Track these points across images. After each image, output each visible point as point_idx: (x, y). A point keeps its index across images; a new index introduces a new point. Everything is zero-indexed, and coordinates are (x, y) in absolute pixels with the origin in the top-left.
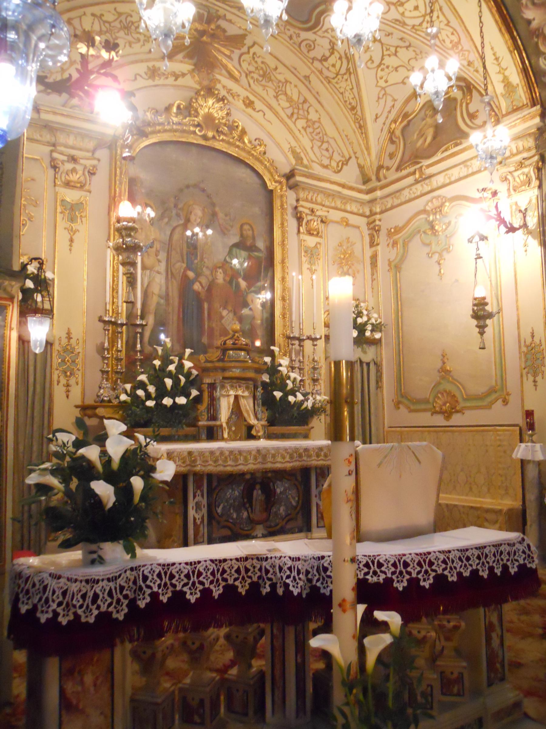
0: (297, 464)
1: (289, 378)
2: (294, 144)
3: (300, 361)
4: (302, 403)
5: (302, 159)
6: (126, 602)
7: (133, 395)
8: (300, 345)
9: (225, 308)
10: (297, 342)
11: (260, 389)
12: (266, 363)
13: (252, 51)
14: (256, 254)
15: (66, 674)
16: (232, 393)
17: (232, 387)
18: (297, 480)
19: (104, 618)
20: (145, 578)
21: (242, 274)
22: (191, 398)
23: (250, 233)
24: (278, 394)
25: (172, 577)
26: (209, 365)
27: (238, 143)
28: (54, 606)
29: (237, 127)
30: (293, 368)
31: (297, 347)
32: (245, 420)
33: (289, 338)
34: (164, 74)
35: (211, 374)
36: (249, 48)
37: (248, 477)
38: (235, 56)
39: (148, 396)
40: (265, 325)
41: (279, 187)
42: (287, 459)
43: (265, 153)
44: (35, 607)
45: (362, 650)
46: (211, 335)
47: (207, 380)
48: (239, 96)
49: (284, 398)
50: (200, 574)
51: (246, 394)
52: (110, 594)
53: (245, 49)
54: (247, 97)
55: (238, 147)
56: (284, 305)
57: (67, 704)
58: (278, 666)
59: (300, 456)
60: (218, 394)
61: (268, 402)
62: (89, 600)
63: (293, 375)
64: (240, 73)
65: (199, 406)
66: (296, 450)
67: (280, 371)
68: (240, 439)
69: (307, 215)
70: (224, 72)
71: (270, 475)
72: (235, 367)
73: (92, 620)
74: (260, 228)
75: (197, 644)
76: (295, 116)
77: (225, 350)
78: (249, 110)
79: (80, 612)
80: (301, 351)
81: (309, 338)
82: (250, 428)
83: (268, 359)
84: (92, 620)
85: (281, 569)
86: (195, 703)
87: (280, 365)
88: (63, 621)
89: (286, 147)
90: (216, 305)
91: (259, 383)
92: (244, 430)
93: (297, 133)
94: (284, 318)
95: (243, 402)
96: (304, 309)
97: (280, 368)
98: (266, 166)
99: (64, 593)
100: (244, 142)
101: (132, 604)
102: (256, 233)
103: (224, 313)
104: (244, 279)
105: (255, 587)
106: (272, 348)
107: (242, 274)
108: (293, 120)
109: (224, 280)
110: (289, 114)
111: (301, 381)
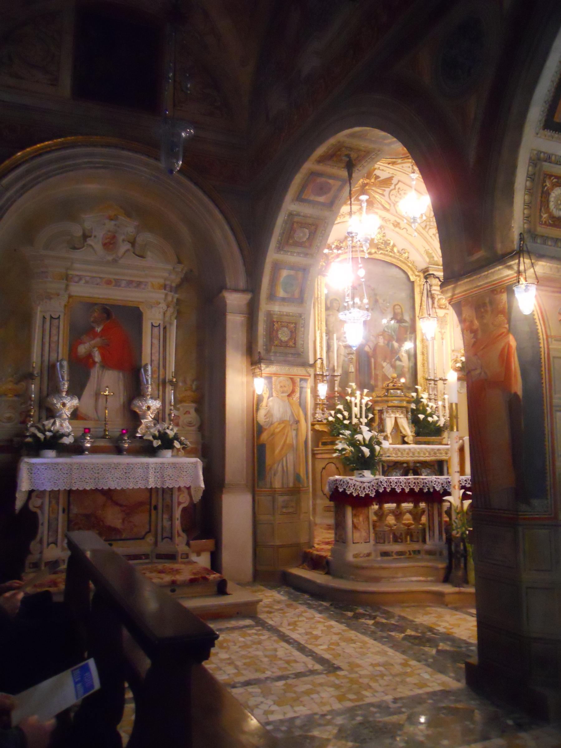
0: (433, 458)
1: (428, 406)
2: (427, 247)
3: (435, 395)
4: (437, 421)
5: (433, 257)
6: (375, 491)
7: (336, 417)
8: (435, 384)
9: (385, 361)
10: (432, 382)
11: (410, 413)
12: (413, 397)
13: (397, 187)
14: (404, 324)
15: (354, 516)
16: (393, 415)
17: (393, 412)
18: (435, 469)
19: (367, 495)
20: (381, 482)
21: (395, 338)
22: (369, 418)
23: (399, 311)
24: (421, 416)
25: (390, 483)
26: (379, 399)
27: (391, 254)
28: (352, 489)
29: (390, 243)
30: (430, 399)
31: (433, 385)
32: (401, 433)
33: (427, 379)
34: (343, 215)
35: (381, 404)
37: (405, 465)
38: (386, 193)
39: (344, 418)
40: (411, 371)
41: (418, 279)
42: (427, 455)
43: (408, 258)
44: (345, 489)
45: (462, 504)
46: (376, 380)
47: (378, 408)
48: (390, 221)
49: (425, 419)
50: (400, 483)
51: (402, 416)
52: (369, 488)
53: (392, 187)
54: (396, 221)
55: (391, 256)
56: (423, 358)
57: (355, 527)
58: (431, 522)
59: (435, 453)
60: (385, 416)
61: (415, 422)
62: (362, 489)
63: (430, 404)
64: (389, 204)
65: (373, 424)
66: (433, 449)
67: (422, 402)
68: (398, 444)
69: (438, 295)
70: (380, 206)
71: (418, 465)
72: (395, 400)
73: (363, 496)
74: (406, 307)
75: (399, 512)
76: (428, 227)
77: (388, 390)
78: (397, 229)
79: (359, 493)
80: (435, 388)
81: (441, 379)
82: (404, 437)
83: (414, 394)
84: (363, 496)
85: (432, 482)
86: (398, 535)
87: (422, 398)
88: (355, 495)
89: (422, 251)
90: (379, 359)
91: (410, 410)
92: (400, 439)
93: (430, 240)
94: (424, 366)
95: (399, 421)
96: (436, 359)
97: (422, 400)
98: (409, 267)
99: (354, 485)
100: (394, 253)
101: (377, 492)
102: (403, 310)
103: (385, 364)
104: (397, 341)
105: (421, 490)
106: (417, 387)
107: (395, 338)
108: (427, 230)
109: (384, 343)
110: (424, 226)
111: (436, 407)
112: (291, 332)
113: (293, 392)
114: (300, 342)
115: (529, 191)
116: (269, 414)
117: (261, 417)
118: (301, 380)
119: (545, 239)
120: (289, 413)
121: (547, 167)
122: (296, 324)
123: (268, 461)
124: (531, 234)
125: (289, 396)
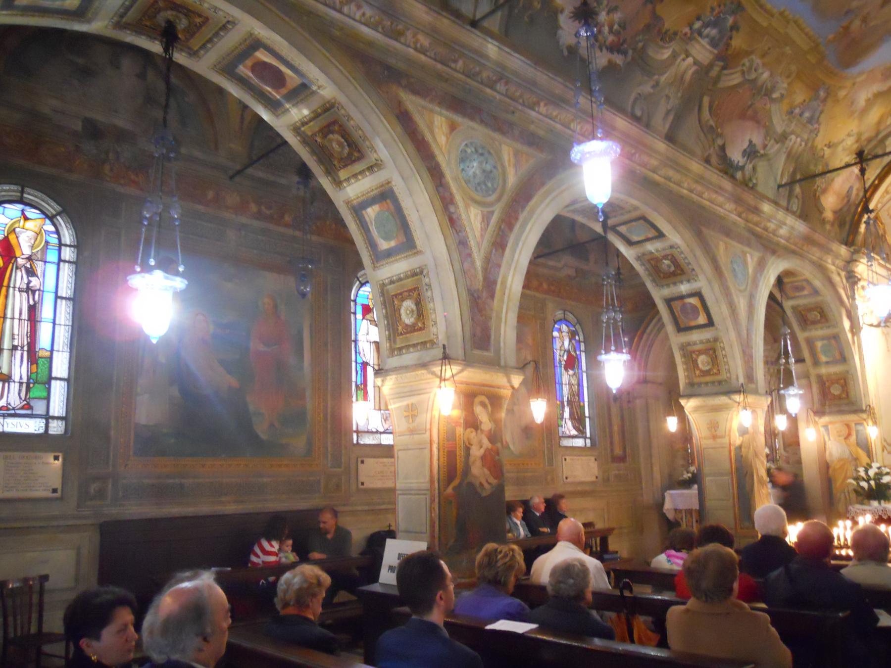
112: (842, 387)
113: (849, 435)
114: (852, 394)
115: (685, 363)
116: (831, 454)
117: (828, 458)
118: (856, 424)
119: (699, 384)
120: (848, 452)
121: (689, 348)
122: (845, 380)
123: (834, 491)
124: (691, 384)
125: (846, 438)
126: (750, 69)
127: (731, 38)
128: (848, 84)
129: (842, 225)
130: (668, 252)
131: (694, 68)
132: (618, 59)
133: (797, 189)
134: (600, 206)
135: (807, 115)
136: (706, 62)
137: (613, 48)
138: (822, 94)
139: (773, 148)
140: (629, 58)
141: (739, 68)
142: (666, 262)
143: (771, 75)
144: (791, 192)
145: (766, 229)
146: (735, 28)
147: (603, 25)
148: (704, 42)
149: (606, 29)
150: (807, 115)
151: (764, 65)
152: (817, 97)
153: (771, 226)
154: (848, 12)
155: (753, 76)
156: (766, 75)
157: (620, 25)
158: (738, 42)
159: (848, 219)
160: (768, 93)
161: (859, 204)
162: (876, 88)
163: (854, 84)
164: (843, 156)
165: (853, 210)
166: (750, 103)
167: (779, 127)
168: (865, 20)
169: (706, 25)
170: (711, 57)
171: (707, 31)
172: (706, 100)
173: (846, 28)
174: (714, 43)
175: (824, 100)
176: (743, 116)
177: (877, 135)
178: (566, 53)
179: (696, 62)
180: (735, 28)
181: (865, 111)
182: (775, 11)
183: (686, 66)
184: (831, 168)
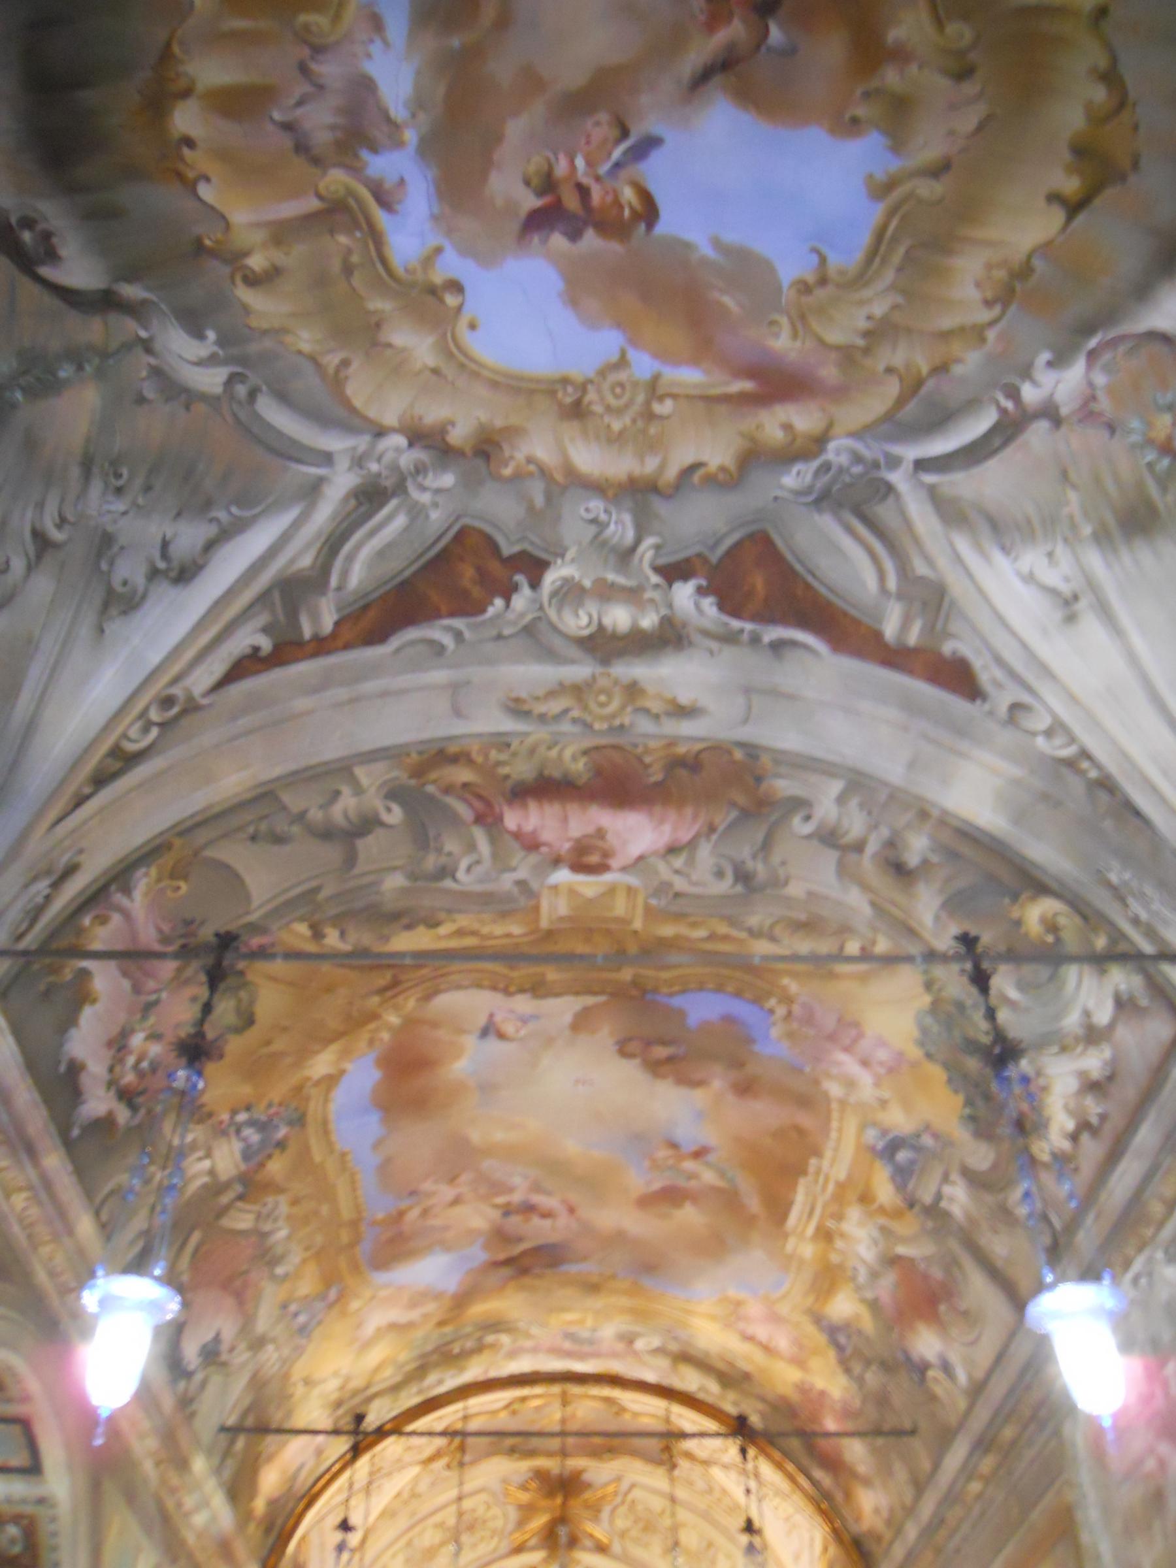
13: (630, 1497)
36: (626, 1494)
126: (269, 1216)
127: (270, 1157)
128: (368, 1293)
129: (268, 1530)
130: (28, 1509)
131: (206, 1179)
132: (123, 1115)
133: (240, 1443)
134: (104, 1413)
135: (302, 1319)
136: (224, 1176)
137: (127, 1096)
138: (333, 1294)
139: (241, 1356)
140: (136, 1121)
141: (256, 1208)
142: (13, 1530)
143: (289, 1238)
144: (232, 1442)
145: (179, 1505)
146: (281, 1145)
147: (131, 1053)
148: (237, 1146)
149: (131, 1060)
150: (302, 1319)
151: (289, 1217)
152: (322, 1296)
153: (189, 1502)
154: (413, 1193)
155: (267, 1227)
156: (282, 1233)
157: (151, 1063)
158: (276, 1167)
159: (279, 1522)
160: (275, 1261)
161: (303, 1497)
162: (396, 1315)
163: (373, 1298)
164: (313, 1410)
165: (291, 1505)
166: (244, 1267)
167: (262, 1325)
168: (425, 1213)
169: (251, 1123)
170: (233, 1172)
171: (248, 1132)
172: (196, 1237)
173: (401, 1214)
174: (247, 1155)
175: (331, 1306)
176: (226, 1285)
177: (367, 1387)
178: (63, 1068)
179: (212, 1172)
180: (281, 1145)
181: (367, 1345)
182: (338, 1147)
183: (197, 1168)
184: (287, 1426)
